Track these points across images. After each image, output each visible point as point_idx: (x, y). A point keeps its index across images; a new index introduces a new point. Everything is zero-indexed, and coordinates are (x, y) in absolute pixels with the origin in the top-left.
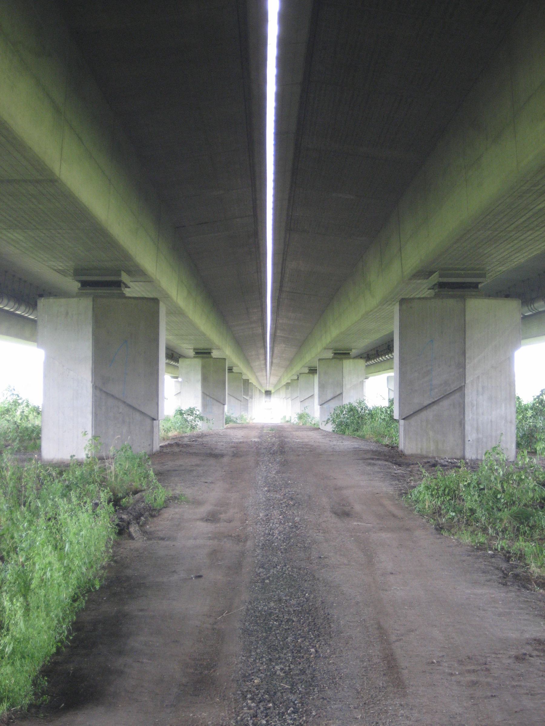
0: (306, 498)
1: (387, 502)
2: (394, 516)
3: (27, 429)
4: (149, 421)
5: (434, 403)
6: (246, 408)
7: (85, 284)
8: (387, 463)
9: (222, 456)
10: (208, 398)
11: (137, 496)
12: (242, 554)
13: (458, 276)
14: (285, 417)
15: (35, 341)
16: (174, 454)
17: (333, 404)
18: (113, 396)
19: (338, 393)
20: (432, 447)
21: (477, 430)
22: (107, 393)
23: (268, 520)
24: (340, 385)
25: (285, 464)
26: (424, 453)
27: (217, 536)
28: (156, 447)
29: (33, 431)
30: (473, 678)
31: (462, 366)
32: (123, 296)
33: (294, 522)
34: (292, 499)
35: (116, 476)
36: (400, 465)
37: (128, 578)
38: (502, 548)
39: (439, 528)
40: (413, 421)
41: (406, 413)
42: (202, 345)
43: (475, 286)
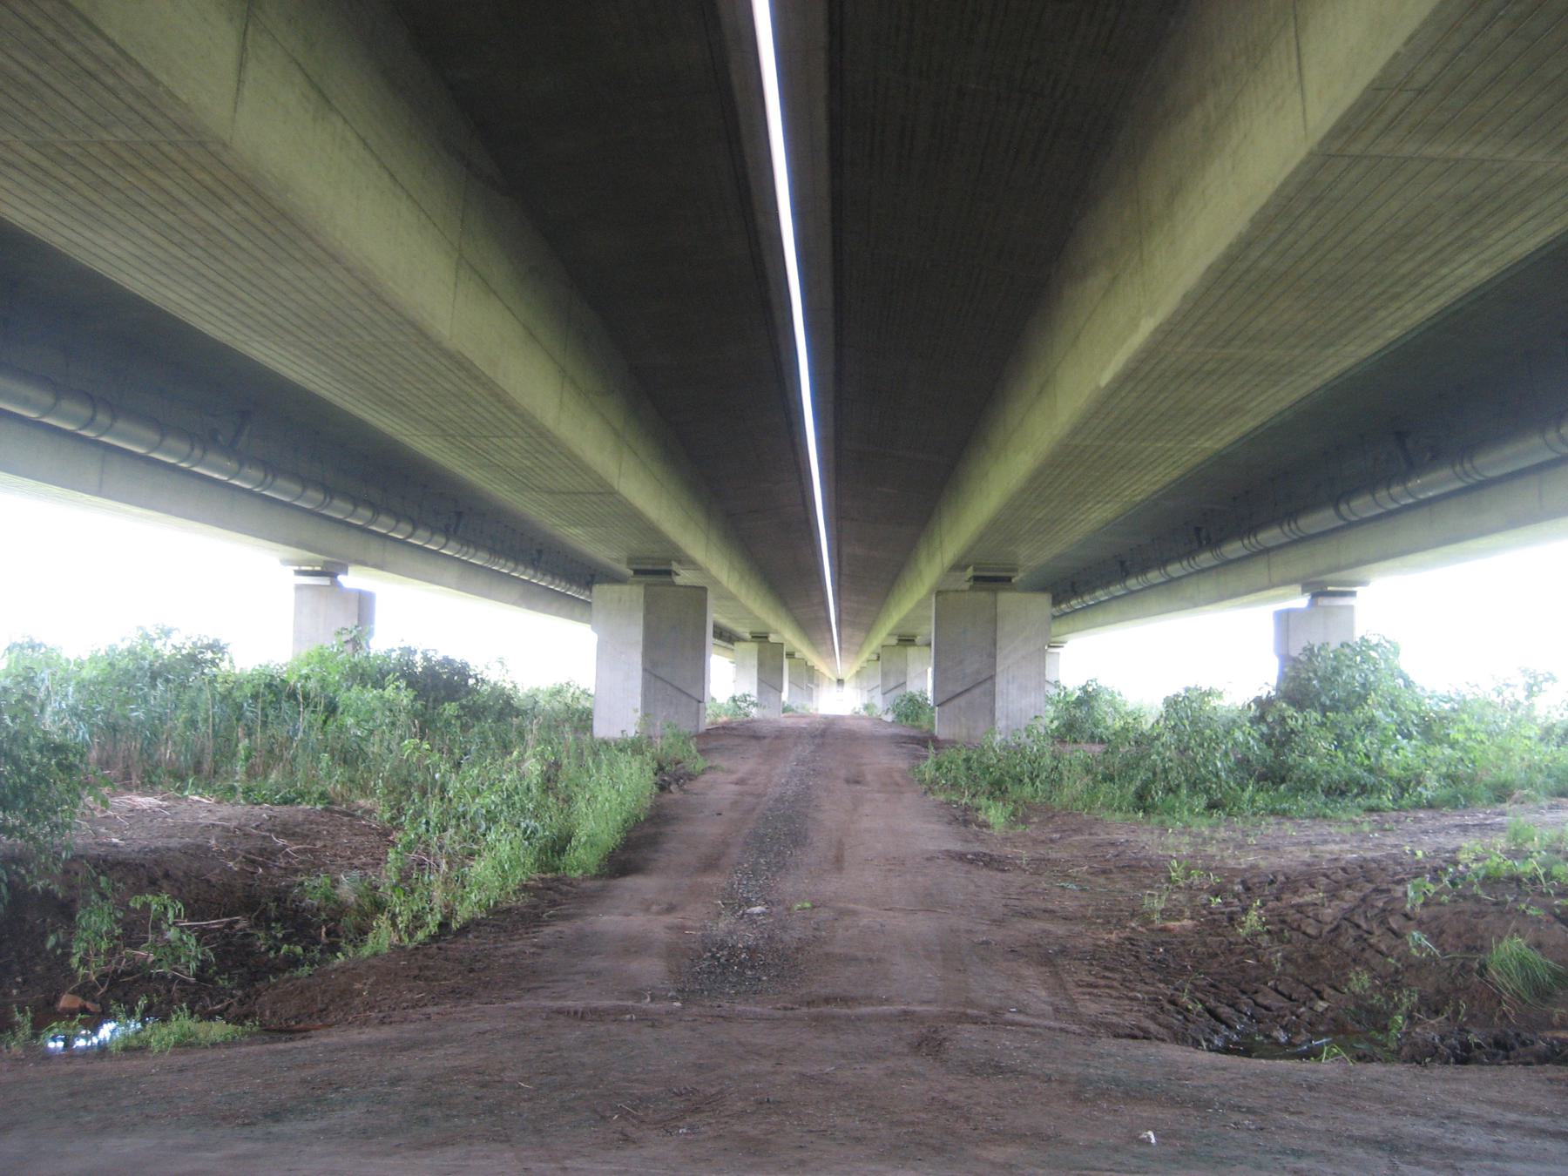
2: (898, 785)
3: (577, 710)
4: (695, 703)
5: (966, 691)
6: (810, 698)
7: (637, 572)
9: (764, 738)
10: (764, 685)
11: (679, 766)
13: (989, 571)
15: (588, 622)
18: (661, 679)
19: (901, 681)
20: (964, 731)
21: (1007, 717)
22: (656, 676)
24: (905, 674)
28: (702, 728)
31: (993, 656)
32: (673, 584)
35: (662, 749)
37: (666, 815)
40: (947, 708)
41: (941, 700)
42: (759, 629)
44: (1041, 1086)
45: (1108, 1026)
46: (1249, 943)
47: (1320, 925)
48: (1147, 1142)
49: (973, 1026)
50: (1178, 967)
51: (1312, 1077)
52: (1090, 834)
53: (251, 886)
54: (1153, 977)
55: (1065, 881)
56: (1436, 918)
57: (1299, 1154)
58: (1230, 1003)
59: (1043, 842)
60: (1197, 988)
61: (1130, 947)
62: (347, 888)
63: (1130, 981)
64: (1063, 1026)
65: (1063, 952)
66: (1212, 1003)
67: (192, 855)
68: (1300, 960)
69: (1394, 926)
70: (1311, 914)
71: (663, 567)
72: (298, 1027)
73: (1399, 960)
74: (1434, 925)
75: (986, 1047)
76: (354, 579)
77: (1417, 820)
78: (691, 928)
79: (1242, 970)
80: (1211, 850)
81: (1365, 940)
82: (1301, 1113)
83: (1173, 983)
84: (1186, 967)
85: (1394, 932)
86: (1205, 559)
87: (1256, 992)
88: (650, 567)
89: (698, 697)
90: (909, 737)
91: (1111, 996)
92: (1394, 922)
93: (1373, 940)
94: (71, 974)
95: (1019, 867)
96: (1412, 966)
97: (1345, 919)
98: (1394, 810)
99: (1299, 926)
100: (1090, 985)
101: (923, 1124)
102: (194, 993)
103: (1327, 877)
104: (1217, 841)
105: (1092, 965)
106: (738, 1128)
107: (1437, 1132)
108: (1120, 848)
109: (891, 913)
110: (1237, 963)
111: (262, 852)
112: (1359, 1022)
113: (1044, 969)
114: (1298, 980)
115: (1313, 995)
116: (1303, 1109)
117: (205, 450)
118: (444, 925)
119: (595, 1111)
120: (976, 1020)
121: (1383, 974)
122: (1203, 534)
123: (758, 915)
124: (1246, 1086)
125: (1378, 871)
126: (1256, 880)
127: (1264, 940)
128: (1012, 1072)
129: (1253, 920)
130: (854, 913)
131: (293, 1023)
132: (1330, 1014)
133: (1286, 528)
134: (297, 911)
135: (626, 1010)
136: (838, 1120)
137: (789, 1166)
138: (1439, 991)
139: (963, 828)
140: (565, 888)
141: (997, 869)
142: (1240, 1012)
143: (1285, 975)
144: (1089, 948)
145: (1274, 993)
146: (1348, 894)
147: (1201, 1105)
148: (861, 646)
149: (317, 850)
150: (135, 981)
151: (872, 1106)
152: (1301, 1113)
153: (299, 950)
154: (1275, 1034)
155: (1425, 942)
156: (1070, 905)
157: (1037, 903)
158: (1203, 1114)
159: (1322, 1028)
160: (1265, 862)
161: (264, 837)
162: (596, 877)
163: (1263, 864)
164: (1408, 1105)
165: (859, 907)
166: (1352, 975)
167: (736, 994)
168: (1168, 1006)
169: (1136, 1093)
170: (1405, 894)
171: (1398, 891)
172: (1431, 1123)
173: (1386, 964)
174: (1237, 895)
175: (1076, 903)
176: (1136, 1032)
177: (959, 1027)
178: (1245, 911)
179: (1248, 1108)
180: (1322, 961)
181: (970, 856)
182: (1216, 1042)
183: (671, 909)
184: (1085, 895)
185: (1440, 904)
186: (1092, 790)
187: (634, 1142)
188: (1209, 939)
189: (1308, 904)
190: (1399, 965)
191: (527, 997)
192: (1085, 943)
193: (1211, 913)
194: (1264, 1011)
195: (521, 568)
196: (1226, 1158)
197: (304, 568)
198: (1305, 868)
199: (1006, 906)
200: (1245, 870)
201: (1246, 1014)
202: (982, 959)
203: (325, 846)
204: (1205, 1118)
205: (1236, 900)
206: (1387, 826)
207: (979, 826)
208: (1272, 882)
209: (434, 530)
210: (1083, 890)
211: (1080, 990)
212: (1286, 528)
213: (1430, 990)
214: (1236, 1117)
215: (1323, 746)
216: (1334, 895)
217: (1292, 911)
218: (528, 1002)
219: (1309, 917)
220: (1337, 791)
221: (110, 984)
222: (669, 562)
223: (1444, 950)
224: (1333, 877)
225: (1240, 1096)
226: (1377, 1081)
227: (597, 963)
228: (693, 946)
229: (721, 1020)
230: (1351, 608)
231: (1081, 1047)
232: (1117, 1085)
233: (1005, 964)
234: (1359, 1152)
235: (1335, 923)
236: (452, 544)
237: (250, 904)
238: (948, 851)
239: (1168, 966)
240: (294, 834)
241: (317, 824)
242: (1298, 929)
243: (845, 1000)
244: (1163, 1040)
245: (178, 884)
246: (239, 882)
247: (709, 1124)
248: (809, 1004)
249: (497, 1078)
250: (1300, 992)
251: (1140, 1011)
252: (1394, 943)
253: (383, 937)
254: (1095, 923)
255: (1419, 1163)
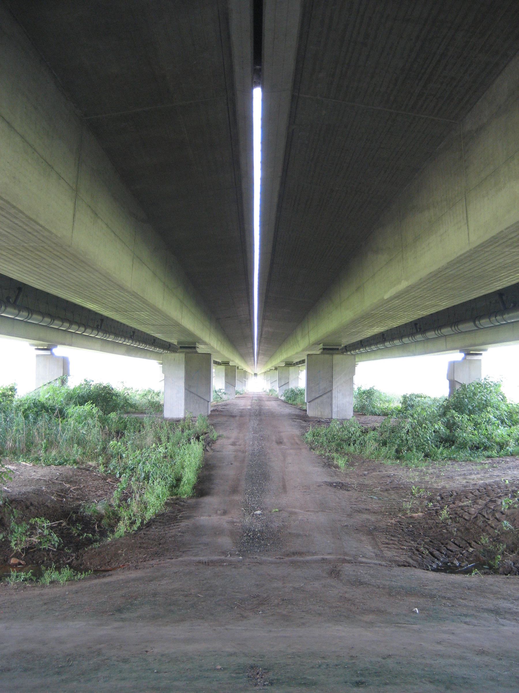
0: (267, 436)
1: (296, 438)
2: (297, 444)
3: (153, 402)
4: (206, 402)
6: (245, 385)
8: (300, 421)
9: (236, 416)
10: (228, 384)
11: (206, 435)
12: (245, 457)
14: (263, 388)
16: (216, 415)
17: (285, 387)
18: (192, 393)
20: (319, 413)
21: (337, 407)
22: (190, 392)
23: (253, 445)
25: (261, 420)
26: (316, 416)
27: (236, 451)
29: (156, 403)
30: (305, 490)
31: (332, 382)
32: (196, 352)
33: (262, 446)
34: (262, 437)
36: (306, 422)
37: (210, 465)
38: (328, 456)
39: (311, 448)
40: (312, 403)
42: (225, 360)
43: (338, 349)
44: (377, 590)
45: (395, 561)
46: (444, 523)
47: (470, 515)
48: (415, 612)
49: (348, 564)
50: (418, 534)
51: (469, 584)
52: (379, 471)
53: (63, 507)
54: (409, 539)
55: (372, 495)
56: (513, 514)
57: (466, 616)
58: (438, 549)
59: (361, 475)
60: (426, 543)
61: (400, 525)
62: (100, 508)
63: (401, 541)
64: (380, 562)
65: (375, 529)
66: (431, 549)
67: (37, 494)
68: (463, 530)
69: (498, 517)
70: (466, 510)
71: (193, 346)
72: (101, 569)
73: (499, 530)
74: (512, 516)
75: (355, 573)
76: (60, 351)
77: (507, 462)
78: (236, 522)
79: (442, 534)
80: (427, 478)
81: (487, 522)
82: (466, 599)
83: (416, 541)
84: (421, 533)
85: (497, 519)
86: (419, 337)
87: (447, 544)
88: (186, 346)
89: (208, 400)
90: (297, 415)
91: (395, 548)
92: (498, 515)
93: (490, 522)
94: (11, 550)
95: (354, 488)
96: (505, 533)
97: (480, 513)
98: (497, 457)
99: (462, 516)
100: (387, 544)
101: (340, 607)
102: (58, 555)
103: (472, 493)
104: (429, 474)
105: (387, 534)
106: (278, 611)
107: (511, 606)
108: (392, 479)
109: (309, 513)
110: (440, 531)
111: (62, 491)
112: (484, 556)
113: (369, 537)
114: (462, 538)
115: (468, 545)
116: (466, 597)
117: (6, 307)
118: (142, 523)
119: (228, 605)
120: (349, 562)
121: (493, 536)
122: (418, 326)
123: (259, 515)
124: (447, 589)
125: (492, 491)
126: (445, 494)
127: (449, 522)
128: (365, 584)
129: (444, 513)
130: (295, 513)
131: (99, 567)
132: (474, 553)
133: (453, 328)
134: (83, 517)
135: (223, 561)
136: (311, 607)
137: (300, 625)
138: (513, 543)
139: (329, 469)
140: (182, 503)
141: (345, 490)
142: (441, 553)
143: (457, 536)
144: (385, 527)
145: (454, 544)
146: (480, 501)
147: (432, 596)
148: (267, 362)
149: (82, 489)
150: (34, 551)
151: (320, 601)
152: (466, 599)
153: (90, 535)
154: (455, 562)
155: (508, 525)
156: (375, 507)
157: (363, 506)
158: (433, 600)
159: (471, 559)
160: (449, 485)
161: (60, 484)
162: (193, 497)
163: (447, 486)
164: (502, 595)
165: (297, 510)
166: (482, 537)
167: (260, 551)
168: (416, 552)
169: (410, 592)
170: (502, 503)
171: (499, 502)
172: (509, 602)
173: (494, 532)
174: (438, 501)
175: (377, 505)
176: (405, 564)
177: (343, 564)
178: (442, 508)
179: (448, 598)
180: (471, 530)
181: (334, 484)
182: (434, 566)
183: (225, 513)
184: (380, 501)
185: (514, 508)
186: (378, 449)
187: (246, 618)
188: (429, 521)
189: (465, 506)
190: (499, 533)
191: (184, 555)
192: (383, 524)
193: (429, 510)
194: (450, 552)
195: (127, 340)
196: (442, 618)
197: (39, 347)
198: (464, 489)
199: (351, 508)
200: (440, 489)
201: (444, 554)
202: (346, 533)
203: (84, 487)
204: (434, 602)
205: (438, 504)
206: (495, 465)
207: (334, 467)
208: (451, 496)
209: (93, 328)
210: (380, 499)
211: (383, 545)
212: (453, 328)
213: (510, 543)
214: (444, 601)
215: (470, 429)
216: (475, 502)
217: (459, 509)
218: (186, 558)
219: (466, 512)
220: (476, 448)
221: (26, 553)
222: (195, 344)
223: (515, 527)
224: (474, 493)
225: (445, 593)
226: (491, 585)
227: (205, 539)
228: (238, 530)
229: (258, 564)
230: (480, 360)
231: (387, 572)
232: (403, 589)
233: (355, 535)
234: (486, 615)
235: (476, 515)
236: (100, 333)
237: (65, 515)
238: (326, 482)
239: (414, 533)
240: (71, 482)
241: (78, 476)
242: (462, 517)
243: (300, 554)
244: (415, 567)
245: (37, 508)
246: (58, 506)
247: (269, 609)
248: (288, 555)
249: (190, 593)
250: (463, 544)
251: (406, 554)
252: (497, 524)
253: (122, 528)
254: (385, 515)
255: (505, 618)
